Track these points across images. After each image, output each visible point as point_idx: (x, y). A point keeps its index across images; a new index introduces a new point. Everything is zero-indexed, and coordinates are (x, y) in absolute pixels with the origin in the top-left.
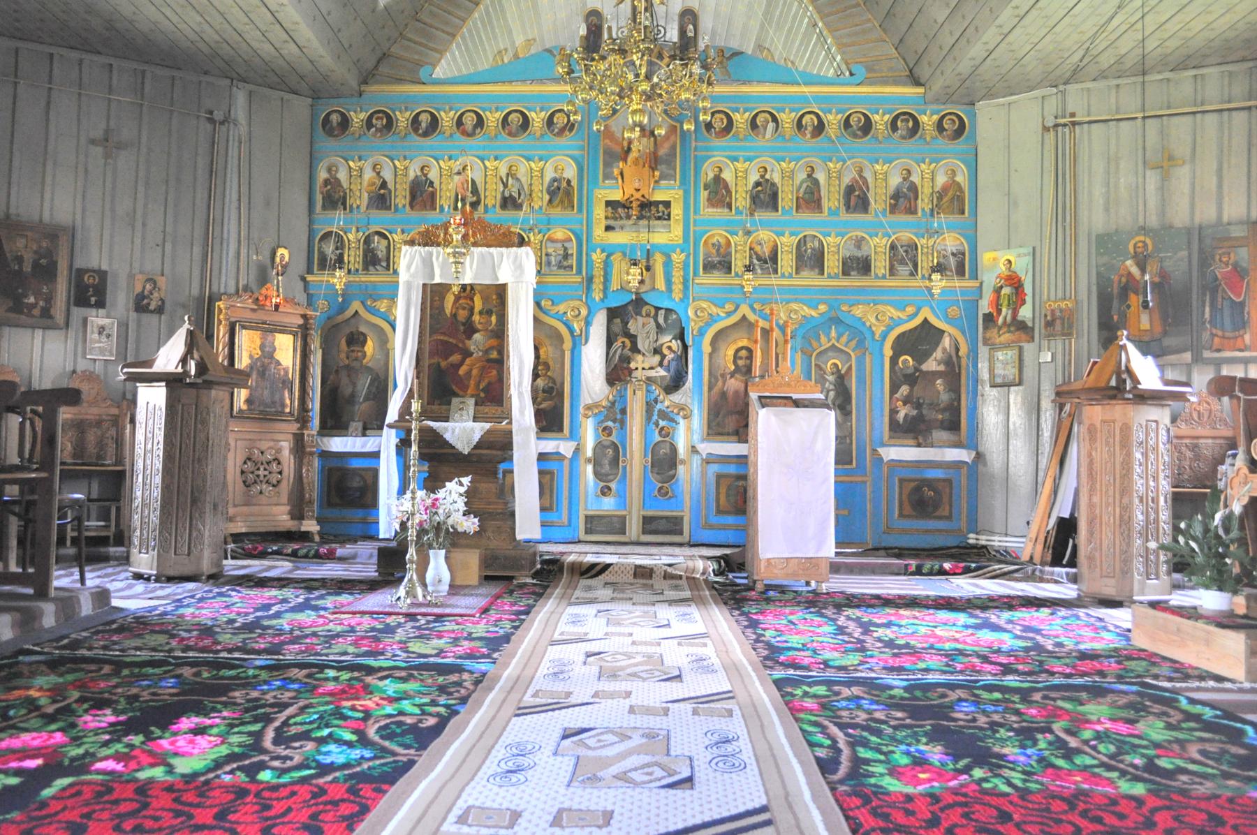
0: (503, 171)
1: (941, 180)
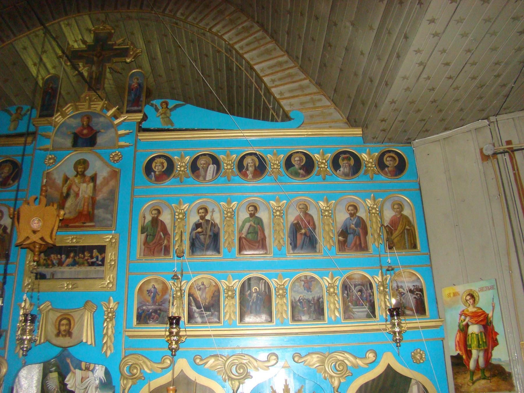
1: (389, 214)
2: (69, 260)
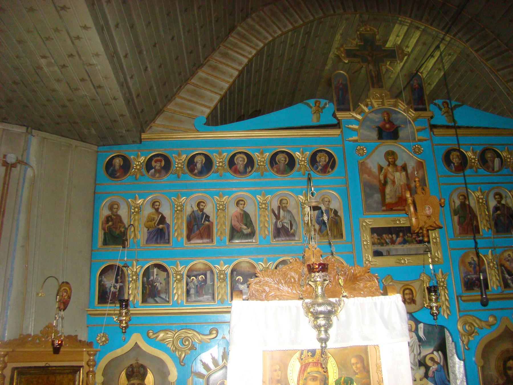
0: (275, 205)
2: (399, 239)
